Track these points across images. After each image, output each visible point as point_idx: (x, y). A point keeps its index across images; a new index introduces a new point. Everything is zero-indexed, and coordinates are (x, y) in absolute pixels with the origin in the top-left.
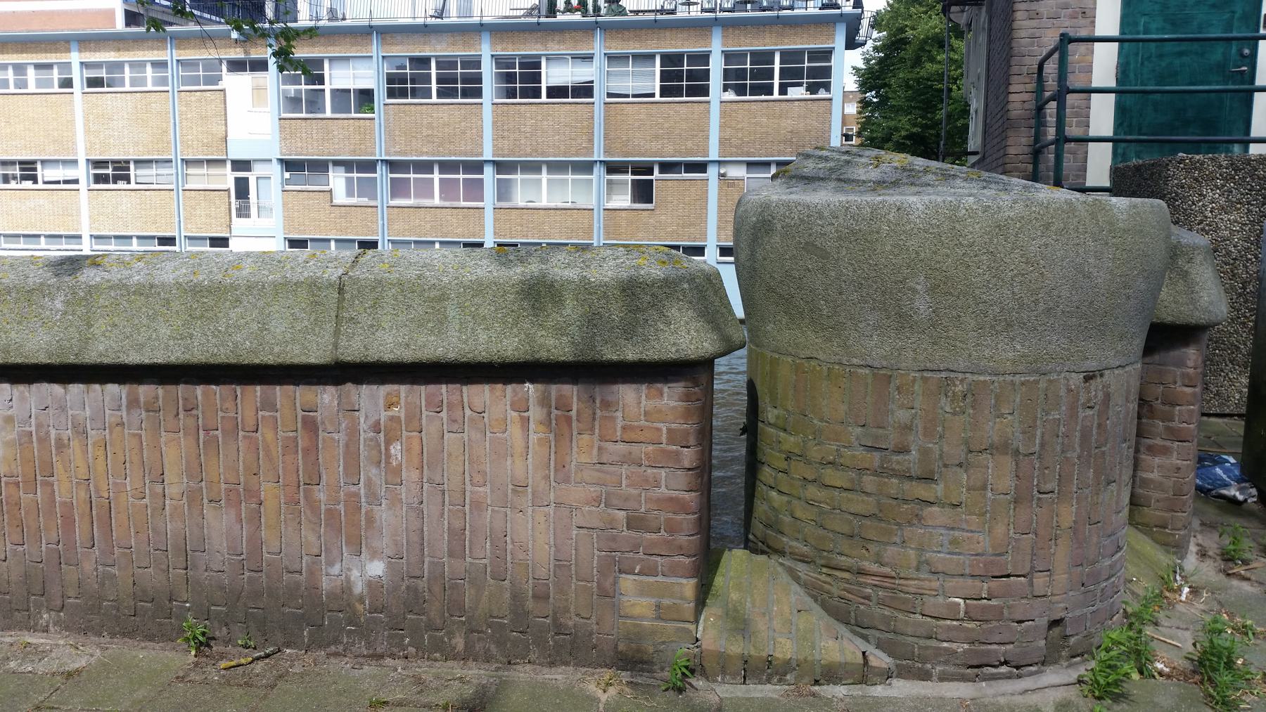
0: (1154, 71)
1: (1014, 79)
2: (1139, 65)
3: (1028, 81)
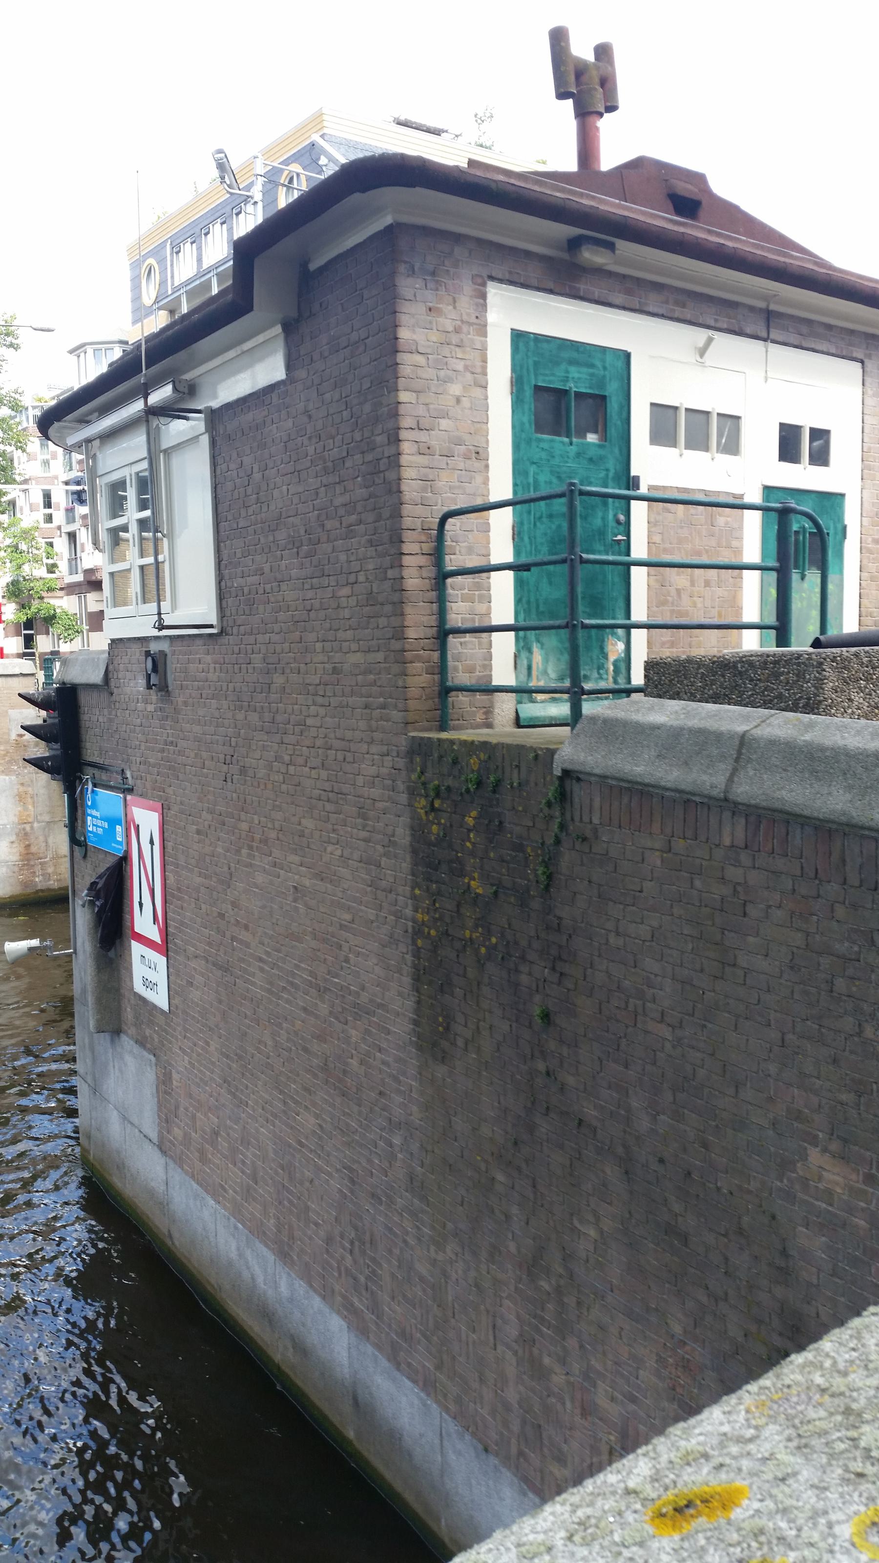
0: (546, 534)
1: (407, 536)
2: (532, 526)
3: (423, 538)
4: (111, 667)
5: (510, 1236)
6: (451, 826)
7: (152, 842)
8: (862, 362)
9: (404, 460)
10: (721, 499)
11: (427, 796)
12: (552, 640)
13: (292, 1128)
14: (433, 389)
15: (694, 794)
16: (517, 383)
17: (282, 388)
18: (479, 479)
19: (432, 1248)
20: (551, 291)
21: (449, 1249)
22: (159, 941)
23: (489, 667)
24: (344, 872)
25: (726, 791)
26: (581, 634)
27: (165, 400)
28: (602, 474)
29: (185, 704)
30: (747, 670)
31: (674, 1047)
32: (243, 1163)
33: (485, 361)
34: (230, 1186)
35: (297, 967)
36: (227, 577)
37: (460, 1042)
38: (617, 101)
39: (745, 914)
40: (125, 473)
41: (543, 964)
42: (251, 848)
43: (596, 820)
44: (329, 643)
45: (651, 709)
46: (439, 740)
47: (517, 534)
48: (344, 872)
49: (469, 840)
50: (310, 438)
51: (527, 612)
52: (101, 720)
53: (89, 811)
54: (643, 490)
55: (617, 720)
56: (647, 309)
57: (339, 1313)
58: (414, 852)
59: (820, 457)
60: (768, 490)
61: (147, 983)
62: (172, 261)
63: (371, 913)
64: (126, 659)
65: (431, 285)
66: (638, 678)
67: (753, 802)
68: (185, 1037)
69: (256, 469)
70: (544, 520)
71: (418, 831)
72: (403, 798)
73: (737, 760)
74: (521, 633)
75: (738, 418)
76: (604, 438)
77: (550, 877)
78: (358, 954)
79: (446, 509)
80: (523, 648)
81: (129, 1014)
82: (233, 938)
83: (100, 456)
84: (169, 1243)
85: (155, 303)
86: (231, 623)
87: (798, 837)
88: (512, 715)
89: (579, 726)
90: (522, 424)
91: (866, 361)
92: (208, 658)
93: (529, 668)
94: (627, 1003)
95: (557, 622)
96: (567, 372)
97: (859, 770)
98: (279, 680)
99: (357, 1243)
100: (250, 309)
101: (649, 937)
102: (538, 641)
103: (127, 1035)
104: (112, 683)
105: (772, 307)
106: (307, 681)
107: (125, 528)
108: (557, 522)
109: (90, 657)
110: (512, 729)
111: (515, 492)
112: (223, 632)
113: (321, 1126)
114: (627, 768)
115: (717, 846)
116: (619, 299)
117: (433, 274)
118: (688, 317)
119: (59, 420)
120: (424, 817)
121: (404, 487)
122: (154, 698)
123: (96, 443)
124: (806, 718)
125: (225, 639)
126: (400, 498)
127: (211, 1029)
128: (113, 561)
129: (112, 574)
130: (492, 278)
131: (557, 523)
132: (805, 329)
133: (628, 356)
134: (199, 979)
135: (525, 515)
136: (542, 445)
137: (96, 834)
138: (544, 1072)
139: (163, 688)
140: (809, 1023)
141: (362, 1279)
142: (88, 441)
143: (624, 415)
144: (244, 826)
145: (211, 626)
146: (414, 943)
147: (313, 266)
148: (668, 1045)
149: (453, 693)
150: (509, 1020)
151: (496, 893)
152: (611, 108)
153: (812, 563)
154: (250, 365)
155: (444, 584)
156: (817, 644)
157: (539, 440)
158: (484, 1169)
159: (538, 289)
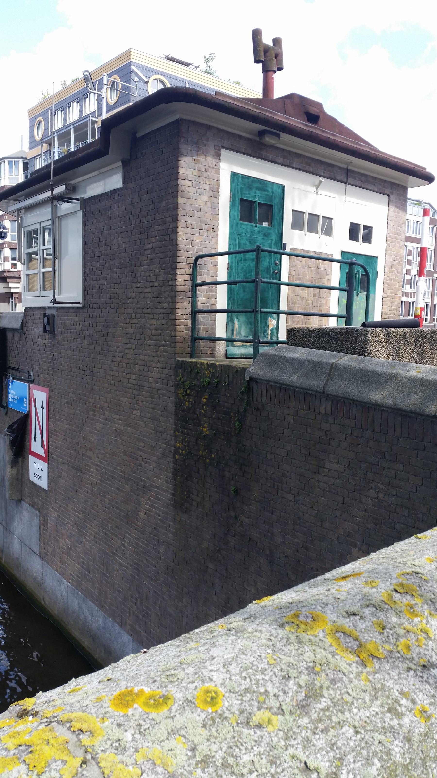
0: (243, 268)
1: (179, 265)
3: (187, 267)
4: (25, 321)
5: (214, 593)
6: (195, 402)
7: (42, 407)
8: (389, 196)
9: (180, 230)
10: (323, 256)
11: (184, 388)
12: (243, 318)
13: (109, 545)
14: (194, 198)
15: (309, 390)
16: (233, 196)
17: (121, 192)
18: (213, 241)
19: (176, 600)
20: (250, 155)
21: (184, 600)
22: (44, 455)
23: (214, 329)
24: (141, 423)
25: (324, 389)
26: (259, 315)
27: (61, 193)
28: (270, 242)
29: (63, 340)
30: (334, 336)
31: (295, 504)
32: (83, 563)
33: (218, 186)
34: (76, 574)
35: (115, 468)
36: (88, 280)
37: (194, 503)
38: (282, 66)
39: (329, 445)
40: (37, 226)
41: (236, 467)
42: (94, 411)
43: (264, 401)
44: (139, 315)
45: (291, 351)
46: (191, 362)
47: (230, 268)
48: (141, 423)
49: (203, 409)
50: (133, 216)
51: (233, 304)
52: (18, 346)
53: (10, 391)
54: (288, 250)
55: (275, 355)
56: (293, 165)
57: (128, 633)
58: (176, 414)
59: (367, 239)
60: (344, 253)
61: (36, 476)
62: (51, 119)
63: (154, 443)
64: (33, 317)
65: (195, 149)
66: (282, 336)
67: (335, 394)
68: (56, 502)
69: (105, 229)
70: (242, 261)
71: (179, 404)
72: (172, 389)
73: (329, 375)
74: (230, 314)
75: (332, 219)
76: (271, 224)
77: (241, 427)
78: (146, 462)
79: (198, 254)
80: (230, 322)
81: (26, 491)
82: (83, 455)
83: (24, 217)
84: (43, 603)
85: (41, 140)
86: (89, 303)
87: (354, 410)
88: (224, 352)
89: (258, 358)
90: (234, 216)
91: (391, 195)
92: (76, 319)
93: (233, 330)
94: (274, 485)
95: (249, 310)
96: (256, 193)
97: (382, 381)
98: (112, 330)
99: (139, 600)
100: (107, 153)
101: (286, 455)
102: (237, 318)
103: (25, 502)
104: (25, 329)
105: (350, 168)
106: (127, 332)
107: (36, 253)
108: (248, 262)
109: (15, 316)
110: (223, 358)
111: (230, 248)
112: (84, 306)
113: (123, 544)
114: (280, 377)
115: (319, 413)
116: (280, 160)
117: (197, 143)
118: (311, 170)
119: (5, 199)
120: (182, 398)
121: (179, 243)
122: (47, 337)
123: (23, 211)
124: (360, 357)
125: (85, 310)
126: (177, 248)
127: (69, 498)
128: (28, 269)
129: (27, 275)
130: (223, 147)
131: (248, 263)
132: (364, 179)
133: (283, 187)
134: (64, 474)
135: (234, 259)
136: (243, 226)
137: (13, 403)
138: (234, 517)
139: (52, 332)
140: (355, 493)
141: (141, 617)
142: (19, 210)
143: (281, 214)
144: (91, 400)
145: (79, 303)
146: (174, 457)
147: (139, 135)
148: (292, 503)
149: (197, 341)
150: (218, 493)
151: (215, 434)
152: (280, 69)
153: (362, 288)
154: (104, 179)
155: (196, 289)
156: (364, 325)
157: (242, 224)
158: (203, 562)
159: (244, 153)
